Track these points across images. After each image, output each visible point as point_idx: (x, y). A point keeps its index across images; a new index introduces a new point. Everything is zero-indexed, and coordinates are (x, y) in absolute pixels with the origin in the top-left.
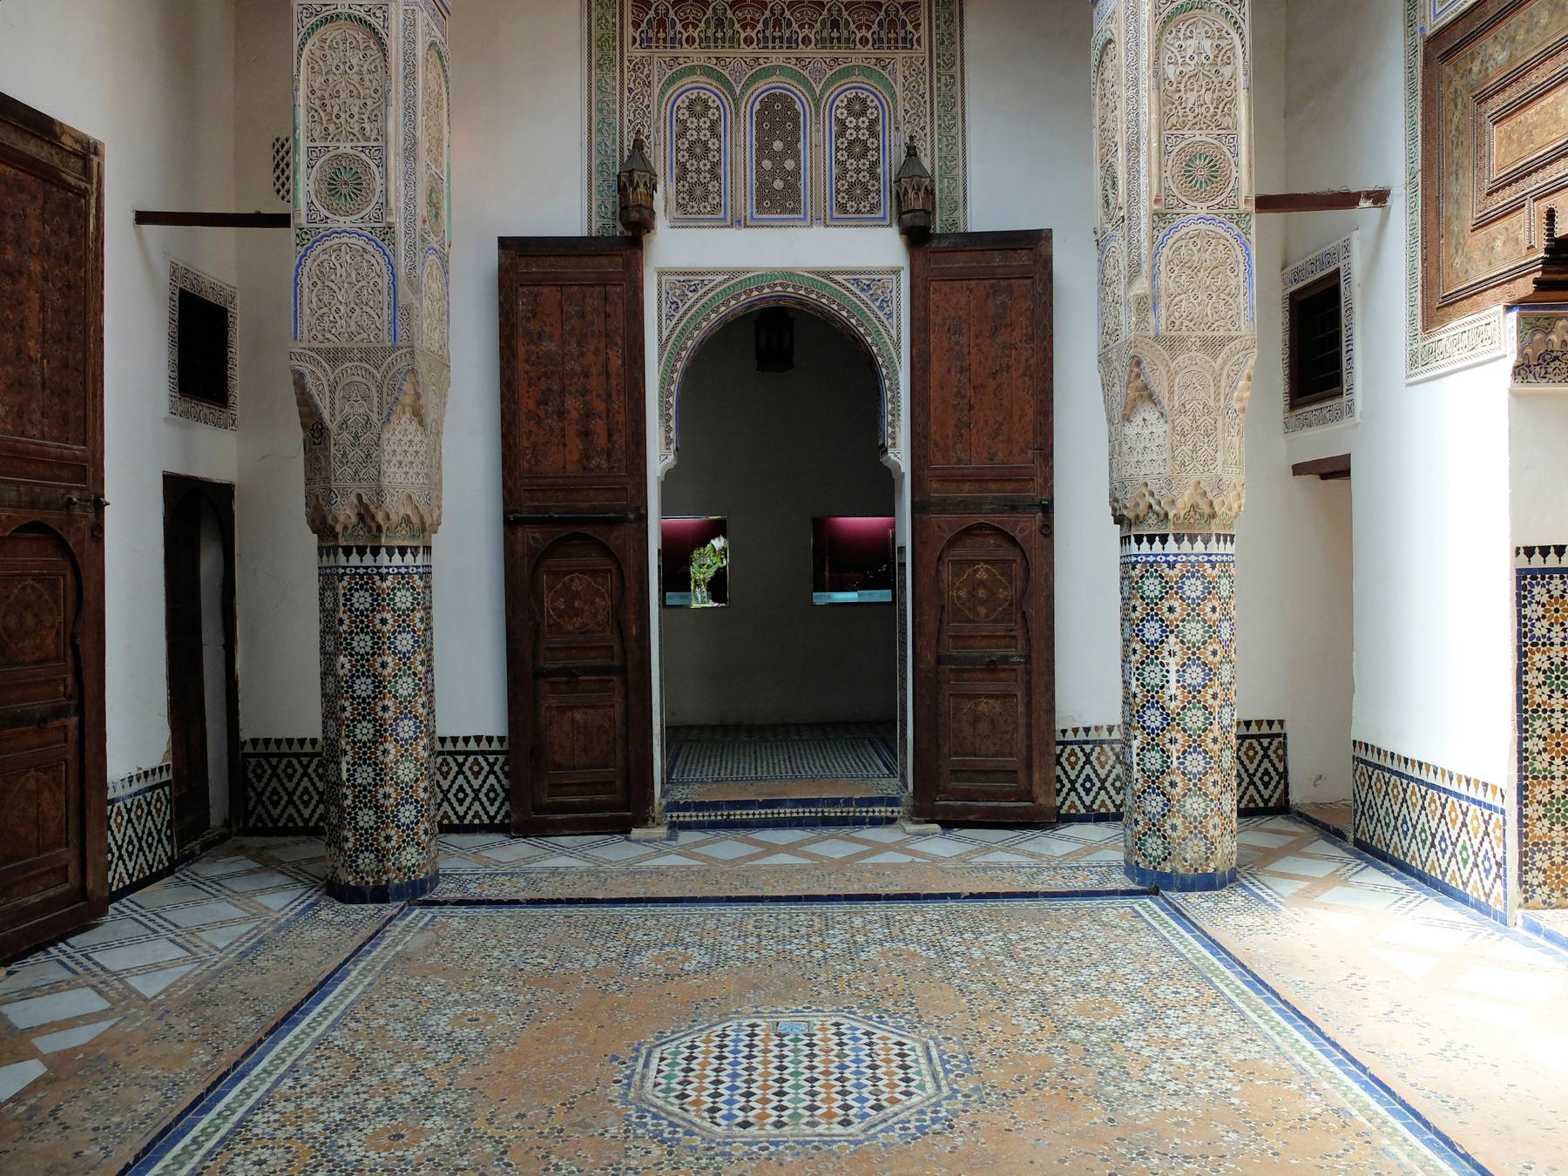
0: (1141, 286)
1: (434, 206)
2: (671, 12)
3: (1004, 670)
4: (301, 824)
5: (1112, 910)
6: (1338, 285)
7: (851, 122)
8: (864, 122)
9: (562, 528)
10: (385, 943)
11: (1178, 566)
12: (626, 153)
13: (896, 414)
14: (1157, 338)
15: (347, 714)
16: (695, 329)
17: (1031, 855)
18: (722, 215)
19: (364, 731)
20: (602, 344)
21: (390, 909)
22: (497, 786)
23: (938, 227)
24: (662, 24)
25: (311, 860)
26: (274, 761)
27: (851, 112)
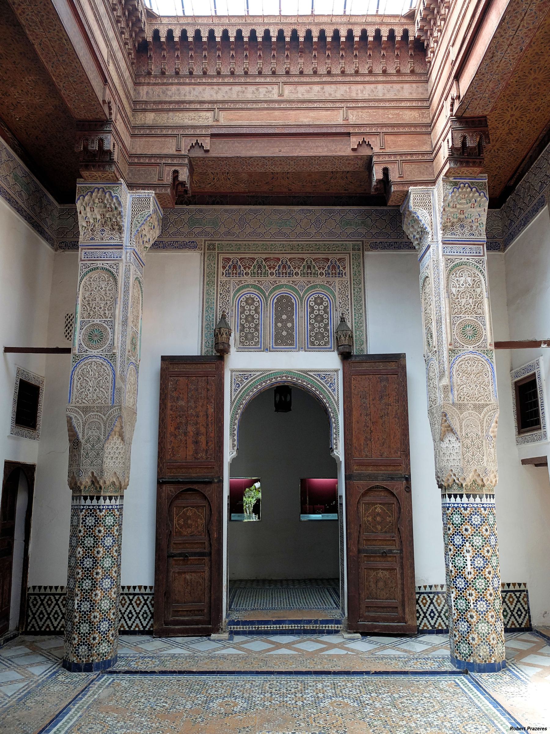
0: (445, 381)
1: (134, 344)
2: (239, 262)
3: (390, 557)
4: (52, 629)
5: (445, 682)
6: (535, 380)
7: (316, 307)
8: (322, 307)
9: (184, 486)
10: (89, 694)
11: (468, 509)
12: (218, 320)
13: (337, 434)
14: (453, 404)
15: (79, 576)
17: (405, 651)
19: (87, 585)
20: (205, 402)
21: (92, 675)
22: (148, 611)
23: (355, 352)
24: (235, 267)
25: (56, 648)
26: (42, 597)
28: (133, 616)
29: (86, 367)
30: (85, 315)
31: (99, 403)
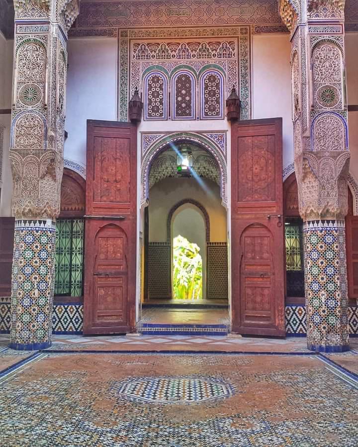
4: (353, 333)
11: (40, 231)
28: (297, 322)
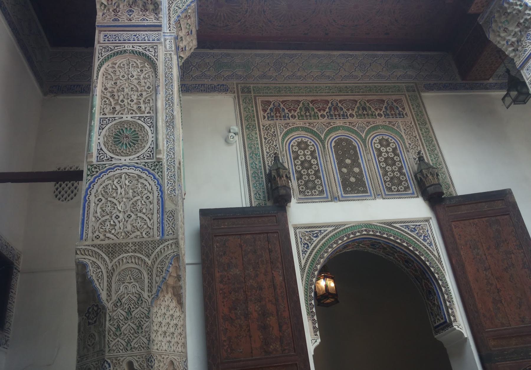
16: (321, 258)
18: (325, 195)
27: (382, 145)
29: (110, 182)
30: (106, 111)
31: (136, 237)
